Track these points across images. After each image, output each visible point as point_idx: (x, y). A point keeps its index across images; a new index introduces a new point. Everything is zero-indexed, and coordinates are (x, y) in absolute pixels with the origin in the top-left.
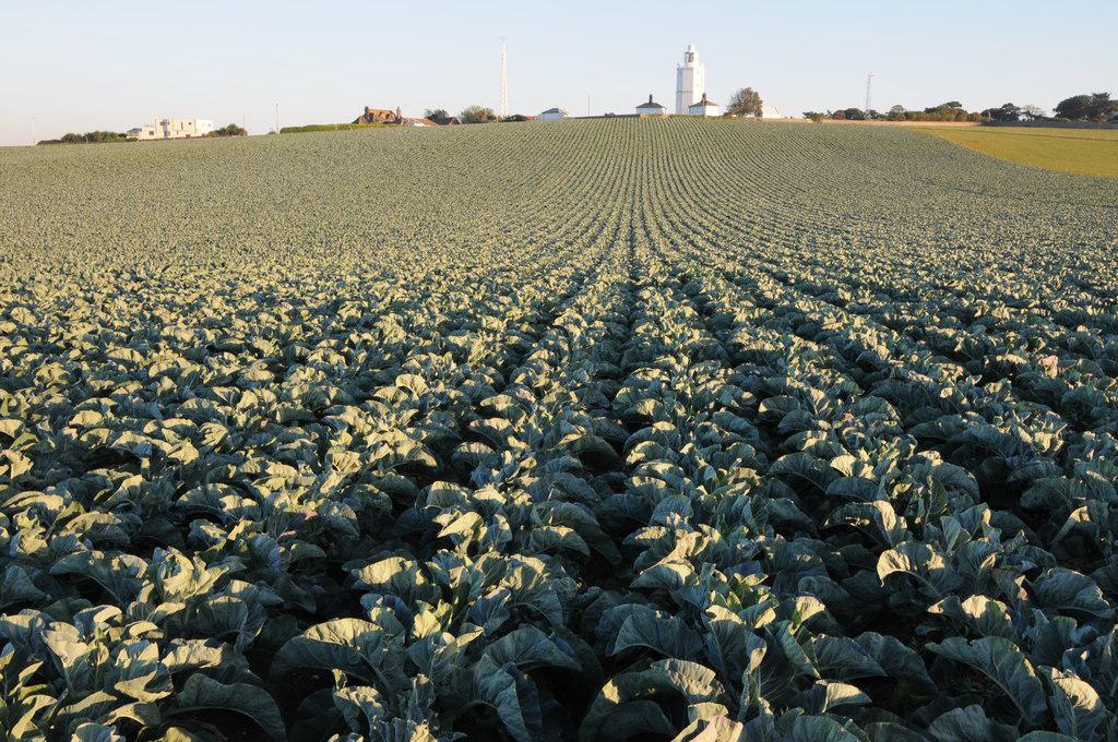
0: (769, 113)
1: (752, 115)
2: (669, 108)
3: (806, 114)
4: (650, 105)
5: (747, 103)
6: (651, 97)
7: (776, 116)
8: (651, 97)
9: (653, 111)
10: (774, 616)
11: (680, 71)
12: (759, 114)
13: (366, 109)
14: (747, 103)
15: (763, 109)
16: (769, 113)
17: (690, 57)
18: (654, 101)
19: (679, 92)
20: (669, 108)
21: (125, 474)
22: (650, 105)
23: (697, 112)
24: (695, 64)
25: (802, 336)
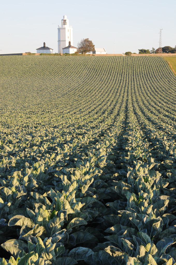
0: (100, 51)
1: (91, 53)
2: (55, 50)
3: (37, 49)
4: (44, 48)
5: (87, 46)
6: (44, 44)
7: (104, 53)
8: (44, 44)
9: (45, 51)
10: (24, 179)
11: (59, 29)
12: (94, 52)
13: (139, 50)
14: (87, 46)
15: (95, 49)
16: (100, 51)
17: (64, 22)
18: (46, 46)
19: (59, 41)
20: (55, 50)
21: (93, 171)
22: (44, 48)
23: (66, 51)
24: (67, 27)
25: (162, 207)
